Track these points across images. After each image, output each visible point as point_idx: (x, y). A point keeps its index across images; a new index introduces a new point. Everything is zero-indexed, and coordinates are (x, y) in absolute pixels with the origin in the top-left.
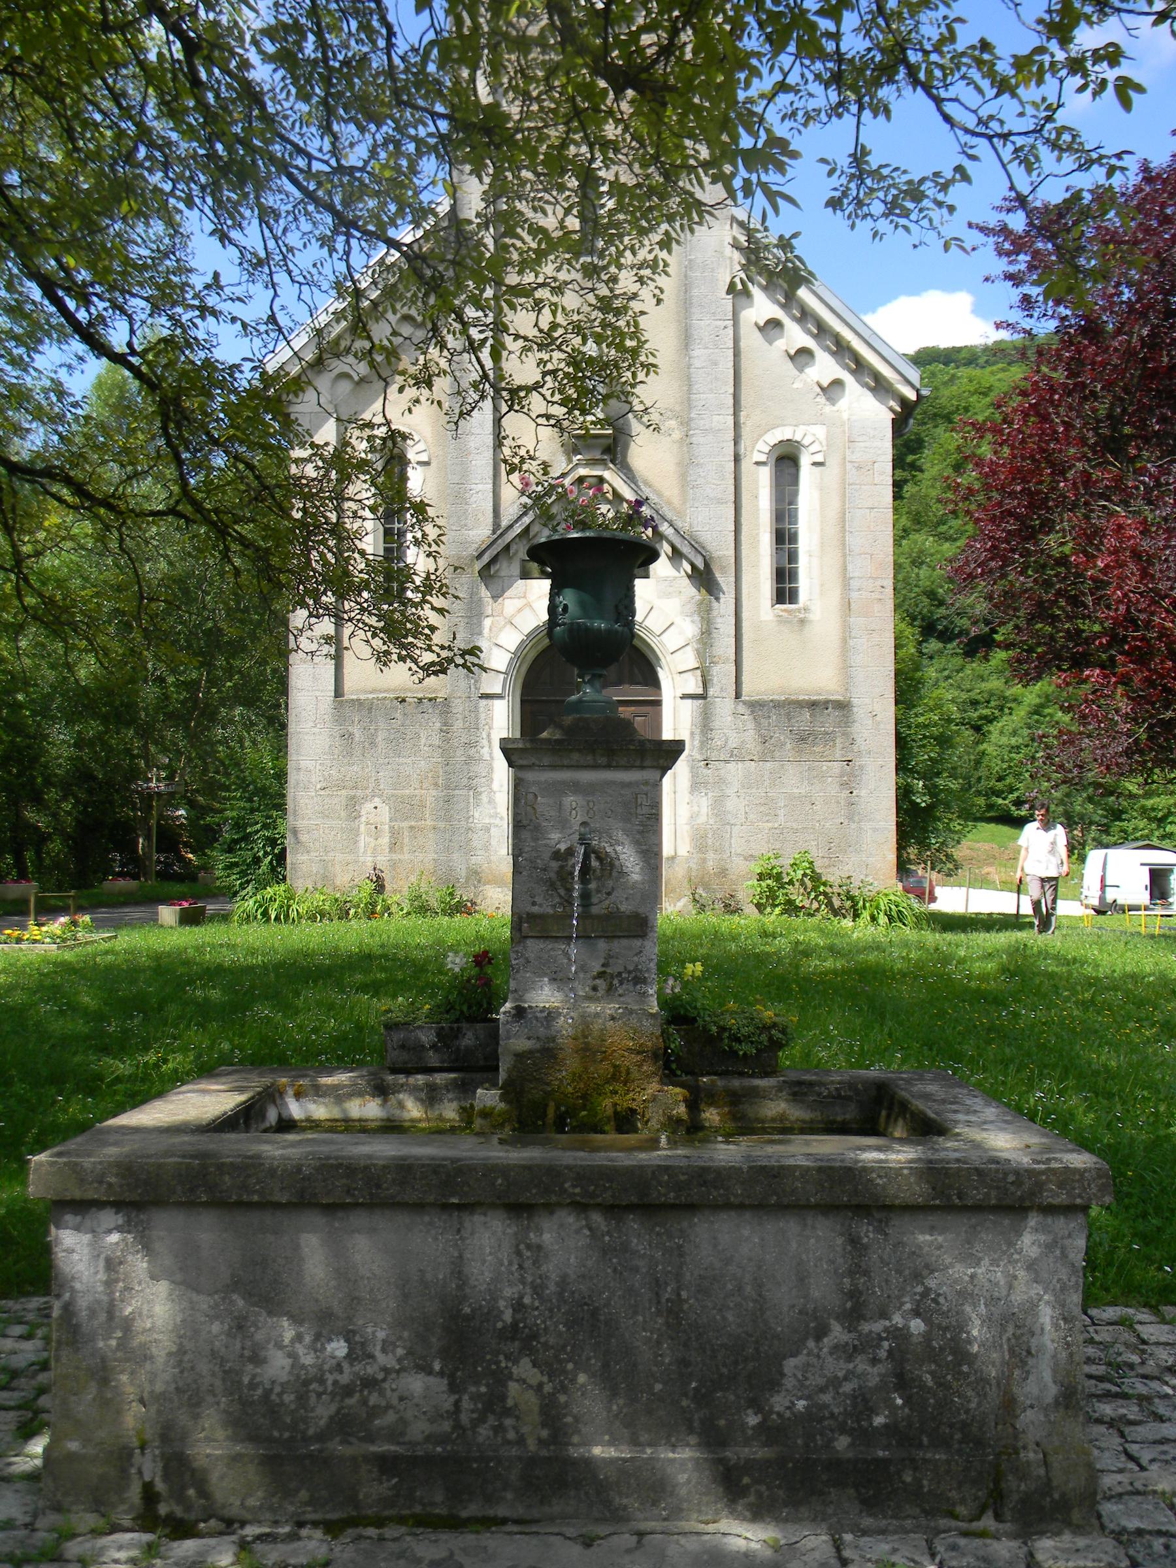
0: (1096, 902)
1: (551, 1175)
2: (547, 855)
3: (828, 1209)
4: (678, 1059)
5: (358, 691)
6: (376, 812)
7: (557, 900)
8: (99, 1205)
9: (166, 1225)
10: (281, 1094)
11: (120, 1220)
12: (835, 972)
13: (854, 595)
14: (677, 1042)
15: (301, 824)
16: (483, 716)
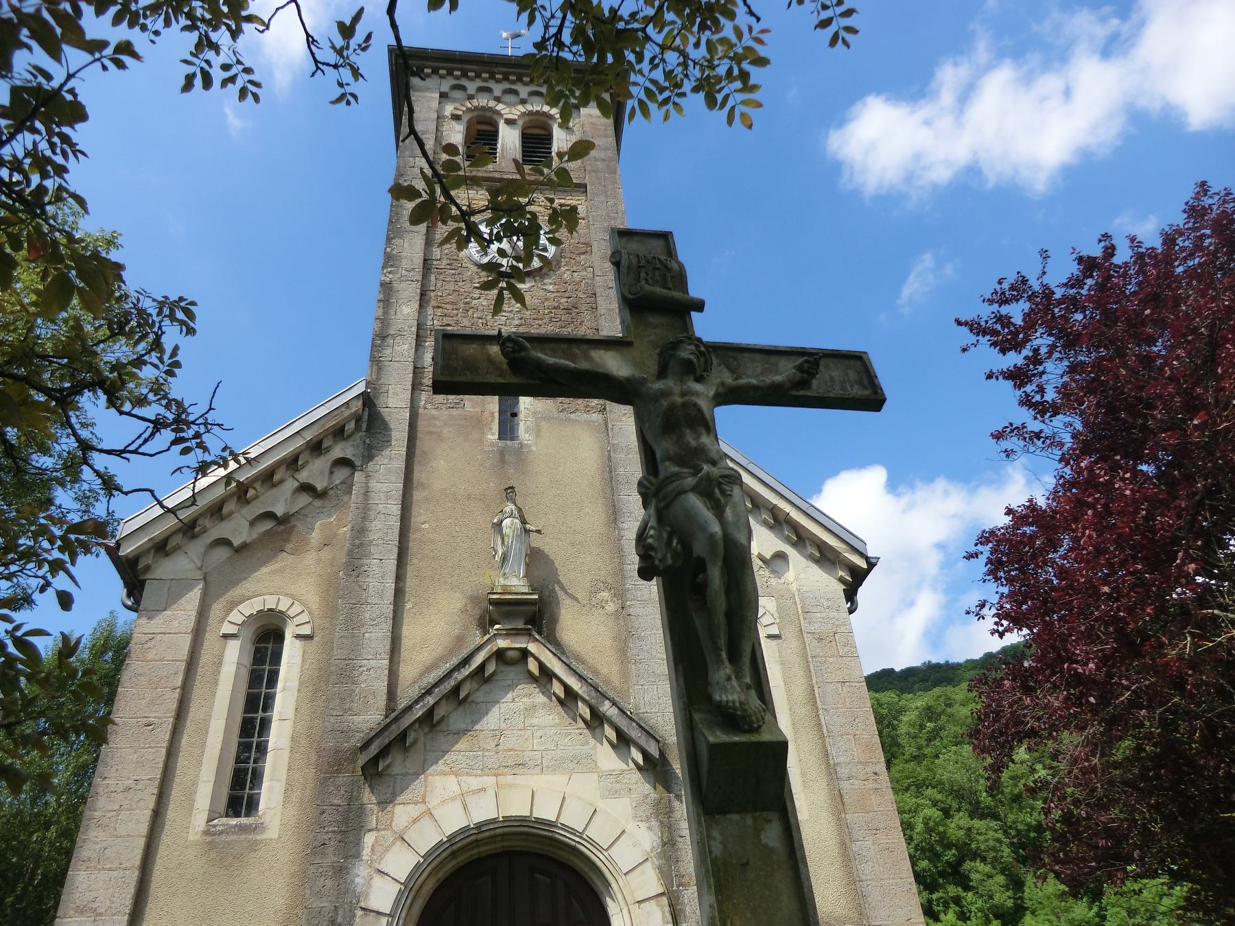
13: (845, 786)
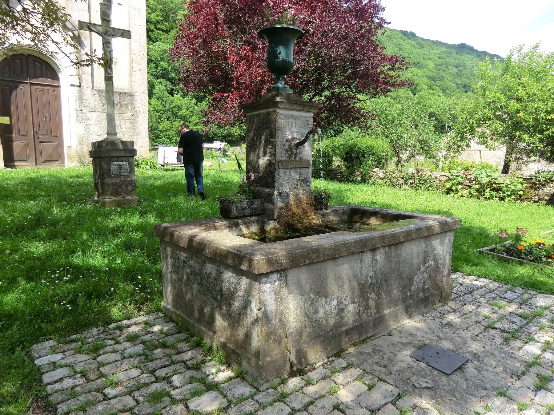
7: (288, 155)
11: (278, 276)
13: (134, 56)
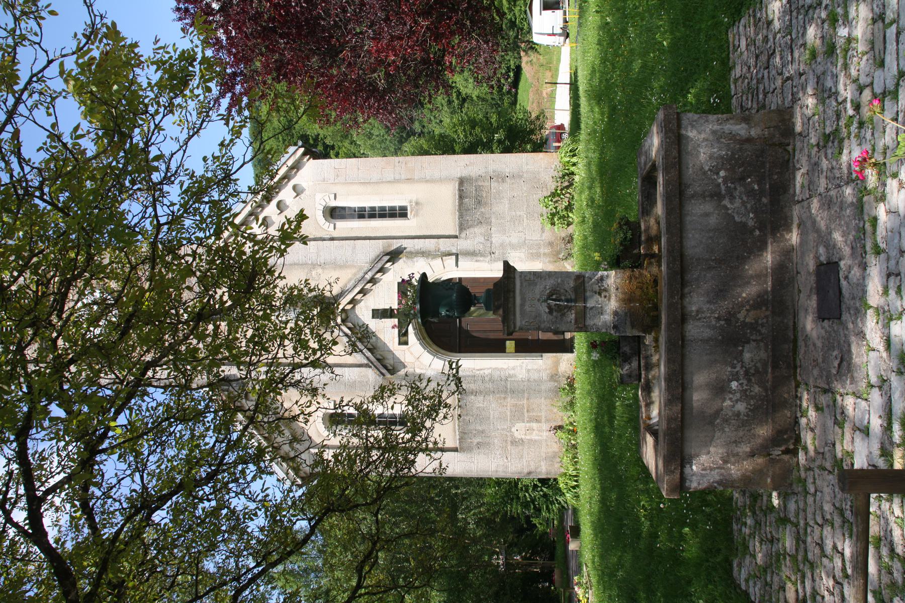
0: (562, 38)
1: (670, 306)
2: (551, 317)
3: (681, 206)
4: (634, 262)
5: (455, 440)
6: (519, 430)
8: (682, 473)
9: (690, 448)
10: (649, 425)
12: (602, 187)
13: (403, 177)
14: (627, 262)
15: (526, 471)
16: (468, 373)
